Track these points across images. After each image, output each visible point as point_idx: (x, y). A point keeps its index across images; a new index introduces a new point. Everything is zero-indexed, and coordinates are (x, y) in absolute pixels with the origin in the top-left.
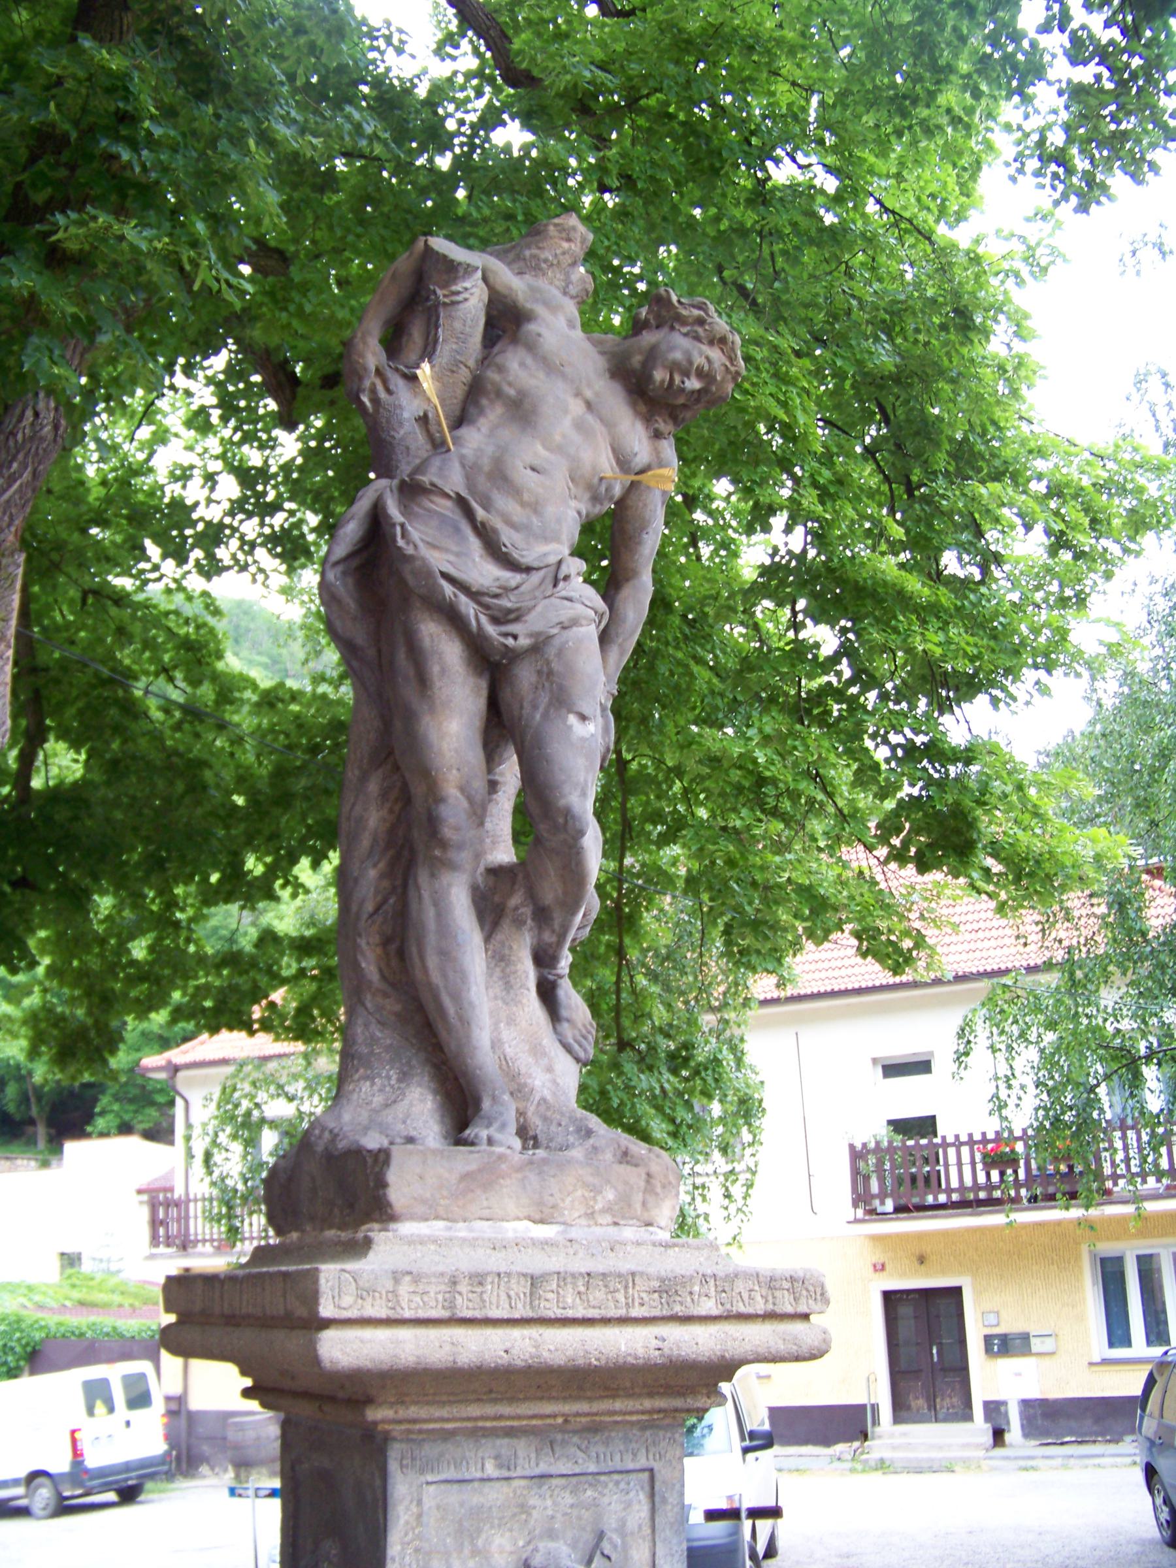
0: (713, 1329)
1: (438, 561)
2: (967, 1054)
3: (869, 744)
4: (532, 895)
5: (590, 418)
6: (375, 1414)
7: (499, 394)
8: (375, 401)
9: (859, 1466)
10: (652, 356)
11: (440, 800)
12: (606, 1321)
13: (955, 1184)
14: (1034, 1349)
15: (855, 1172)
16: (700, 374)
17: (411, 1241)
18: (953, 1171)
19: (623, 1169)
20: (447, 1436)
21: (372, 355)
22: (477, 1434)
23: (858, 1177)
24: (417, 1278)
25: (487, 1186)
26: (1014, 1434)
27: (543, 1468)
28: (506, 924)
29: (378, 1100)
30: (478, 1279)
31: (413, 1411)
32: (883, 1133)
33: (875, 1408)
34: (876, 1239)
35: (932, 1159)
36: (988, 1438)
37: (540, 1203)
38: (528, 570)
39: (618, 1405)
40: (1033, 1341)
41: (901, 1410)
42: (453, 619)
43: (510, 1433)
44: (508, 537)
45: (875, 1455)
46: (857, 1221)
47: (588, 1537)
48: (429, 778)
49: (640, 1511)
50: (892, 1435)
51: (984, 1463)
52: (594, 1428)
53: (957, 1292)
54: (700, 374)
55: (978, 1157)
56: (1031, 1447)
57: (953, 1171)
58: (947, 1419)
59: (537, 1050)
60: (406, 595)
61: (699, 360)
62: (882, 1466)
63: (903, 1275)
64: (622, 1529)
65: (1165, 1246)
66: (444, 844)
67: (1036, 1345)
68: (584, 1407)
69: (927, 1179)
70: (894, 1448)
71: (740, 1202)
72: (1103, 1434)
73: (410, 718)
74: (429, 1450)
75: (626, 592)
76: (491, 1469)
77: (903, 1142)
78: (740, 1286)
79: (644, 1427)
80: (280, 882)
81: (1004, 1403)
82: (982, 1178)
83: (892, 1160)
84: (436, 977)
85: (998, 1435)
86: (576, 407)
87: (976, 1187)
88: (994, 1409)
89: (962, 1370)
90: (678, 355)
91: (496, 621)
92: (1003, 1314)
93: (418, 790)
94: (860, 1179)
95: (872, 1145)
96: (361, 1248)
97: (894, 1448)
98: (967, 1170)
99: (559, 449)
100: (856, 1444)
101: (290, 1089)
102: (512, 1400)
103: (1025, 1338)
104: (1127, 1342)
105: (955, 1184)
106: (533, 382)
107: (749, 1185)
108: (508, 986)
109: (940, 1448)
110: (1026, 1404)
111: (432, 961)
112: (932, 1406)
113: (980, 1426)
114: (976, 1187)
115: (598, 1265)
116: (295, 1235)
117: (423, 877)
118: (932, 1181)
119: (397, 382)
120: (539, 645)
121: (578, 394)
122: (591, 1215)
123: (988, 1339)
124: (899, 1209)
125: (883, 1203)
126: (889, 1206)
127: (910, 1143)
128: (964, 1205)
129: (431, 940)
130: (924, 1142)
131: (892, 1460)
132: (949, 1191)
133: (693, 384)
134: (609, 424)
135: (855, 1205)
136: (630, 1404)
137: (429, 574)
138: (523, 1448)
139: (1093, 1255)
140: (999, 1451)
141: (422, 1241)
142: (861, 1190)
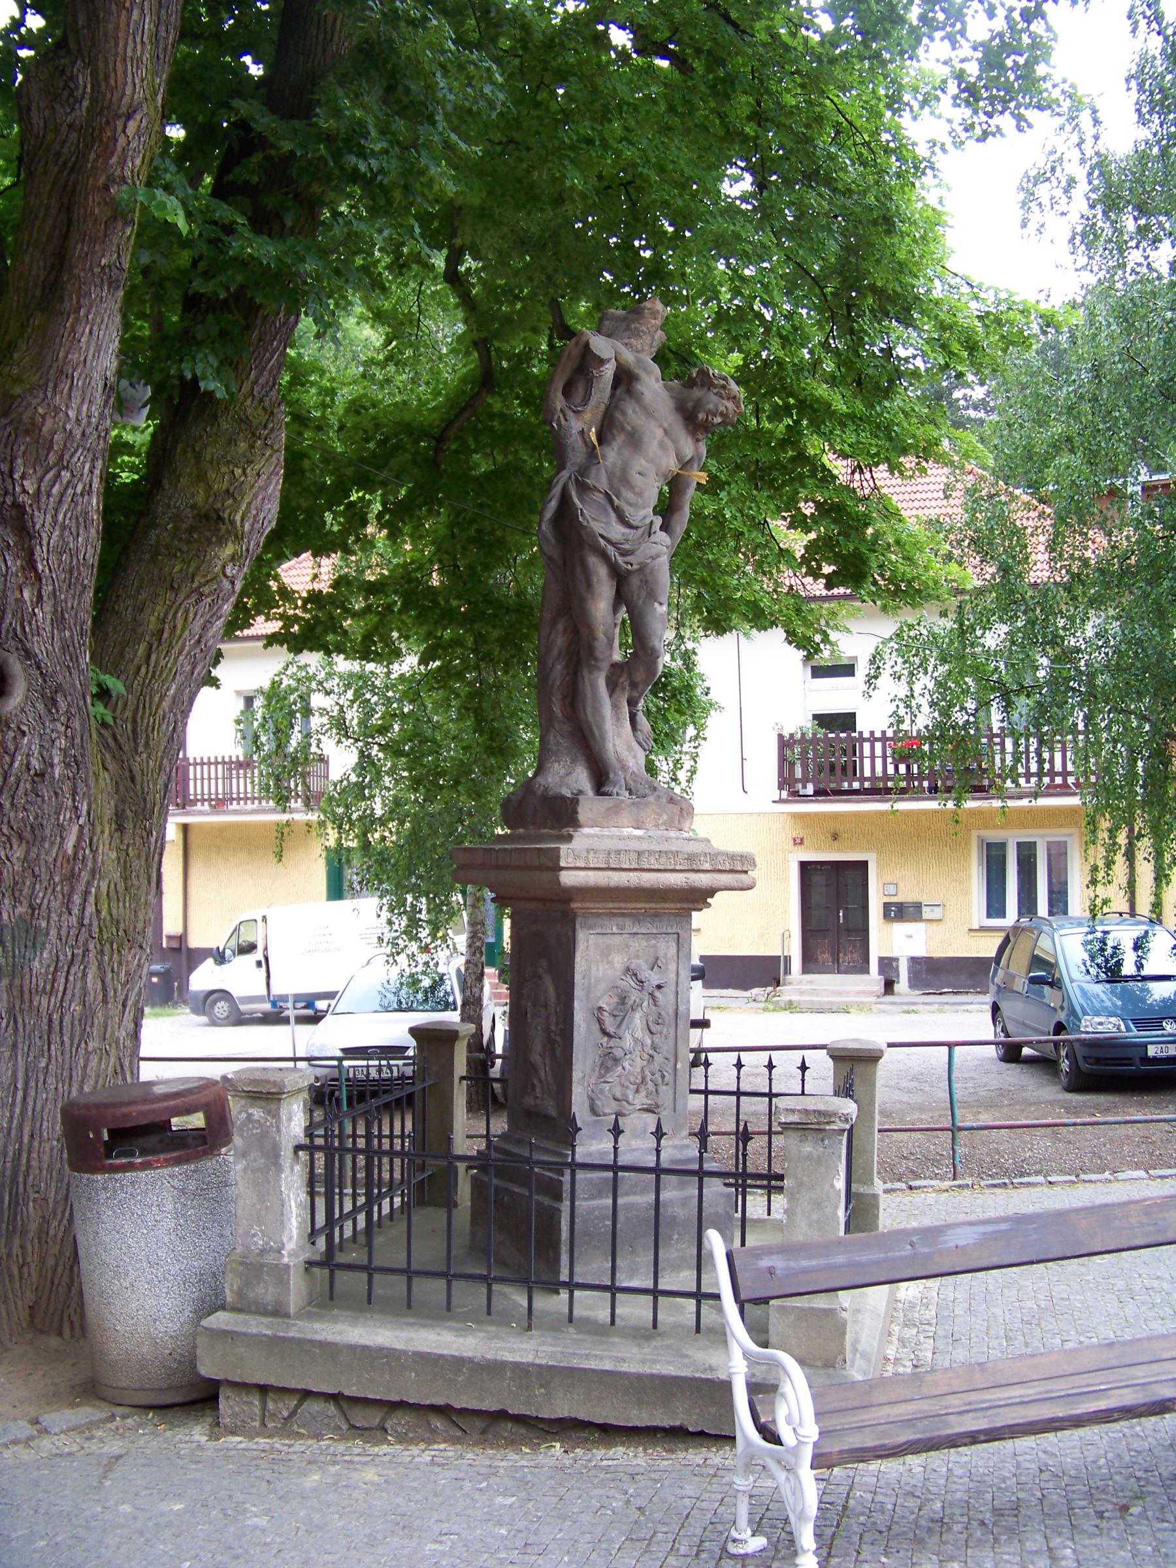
0: (708, 875)
1: (597, 527)
2: (876, 677)
3: (802, 505)
4: (630, 676)
5: (666, 440)
6: (574, 905)
7: (623, 429)
8: (559, 425)
9: (771, 1007)
10: (698, 404)
11: (595, 639)
12: (666, 870)
13: (867, 773)
14: (925, 916)
15: (782, 759)
16: (722, 414)
17: (589, 836)
18: (867, 762)
19: (671, 806)
20: (599, 915)
21: (559, 402)
22: (611, 915)
23: (784, 763)
24: (595, 851)
25: (617, 813)
26: (902, 985)
27: (635, 930)
28: (618, 691)
29: (562, 772)
30: (618, 852)
31: (588, 905)
32: (808, 724)
33: (788, 960)
34: (795, 816)
35: (850, 752)
36: (880, 988)
37: (637, 821)
38: (637, 528)
39: (667, 905)
40: (924, 909)
41: (810, 963)
42: (604, 556)
43: (623, 915)
44: (628, 511)
45: (785, 998)
46: (781, 801)
47: (652, 960)
48: (590, 628)
49: (673, 950)
50: (800, 983)
51: (875, 1007)
52: (656, 915)
53: (864, 865)
54: (722, 414)
55: (889, 752)
56: (916, 996)
57: (867, 762)
58: (846, 972)
59: (630, 749)
60: (581, 542)
61: (721, 408)
62: (790, 1007)
63: (818, 849)
64: (665, 956)
65: (1042, 837)
66: (596, 659)
67: (927, 913)
68: (653, 905)
69: (844, 769)
70: (802, 993)
71: (684, 785)
72: (974, 987)
73: (582, 601)
74: (591, 921)
75: (676, 517)
76: (615, 930)
77: (826, 735)
78: (720, 858)
79: (676, 915)
80: (352, 538)
81: (897, 960)
82: (891, 770)
83: (815, 751)
84: (590, 719)
85: (889, 986)
86: (659, 433)
87: (886, 777)
88: (888, 964)
89: (863, 932)
90: (711, 406)
91: (622, 555)
92: (901, 885)
93: (584, 632)
94: (786, 765)
95: (799, 736)
96: (569, 838)
97: (802, 993)
98: (879, 763)
99: (651, 461)
100: (770, 989)
101: (327, 685)
102: (625, 901)
103: (918, 906)
104: (1002, 913)
105: (867, 773)
106: (640, 422)
107: (693, 772)
108: (618, 719)
109: (840, 994)
110: (914, 961)
111: (589, 711)
112: (836, 960)
113: (874, 977)
114: (886, 777)
115: (664, 847)
116: (521, 830)
117: (585, 673)
118: (850, 770)
119: (570, 415)
120: (642, 568)
121: (661, 426)
122: (657, 826)
123: (887, 906)
124: (817, 793)
125: (805, 787)
126: (810, 789)
127: (832, 735)
128: (877, 791)
129: (589, 703)
130: (843, 735)
131: (799, 1003)
132: (863, 779)
133: (718, 420)
134: (674, 442)
135: (781, 788)
136: (672, 905)
137: (594, 536)
138: (628, 922)
139: (981, 840)
140: (889, 998)
141: (593, 836)
142: (786, 774)
